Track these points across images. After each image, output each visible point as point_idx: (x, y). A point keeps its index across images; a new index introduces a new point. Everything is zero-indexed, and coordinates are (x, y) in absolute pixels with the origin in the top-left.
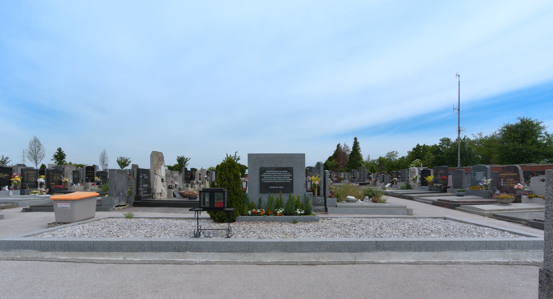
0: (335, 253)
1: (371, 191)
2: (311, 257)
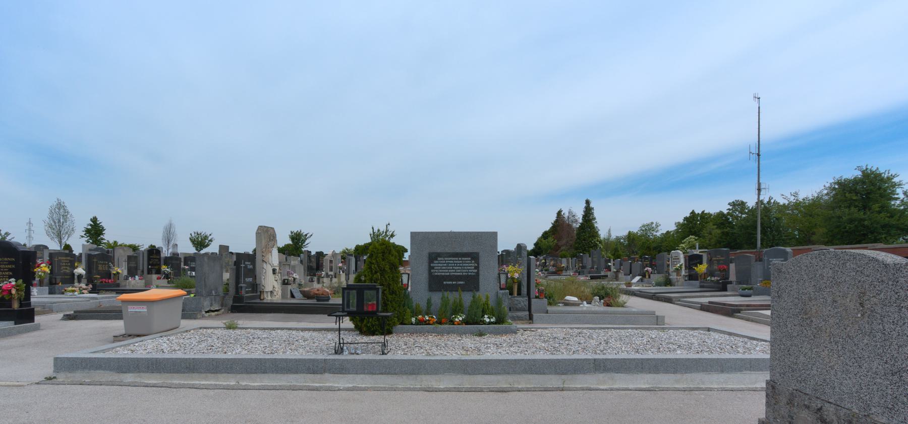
0: (536, 376)
1: (603, 287)
2: (502, 381)
